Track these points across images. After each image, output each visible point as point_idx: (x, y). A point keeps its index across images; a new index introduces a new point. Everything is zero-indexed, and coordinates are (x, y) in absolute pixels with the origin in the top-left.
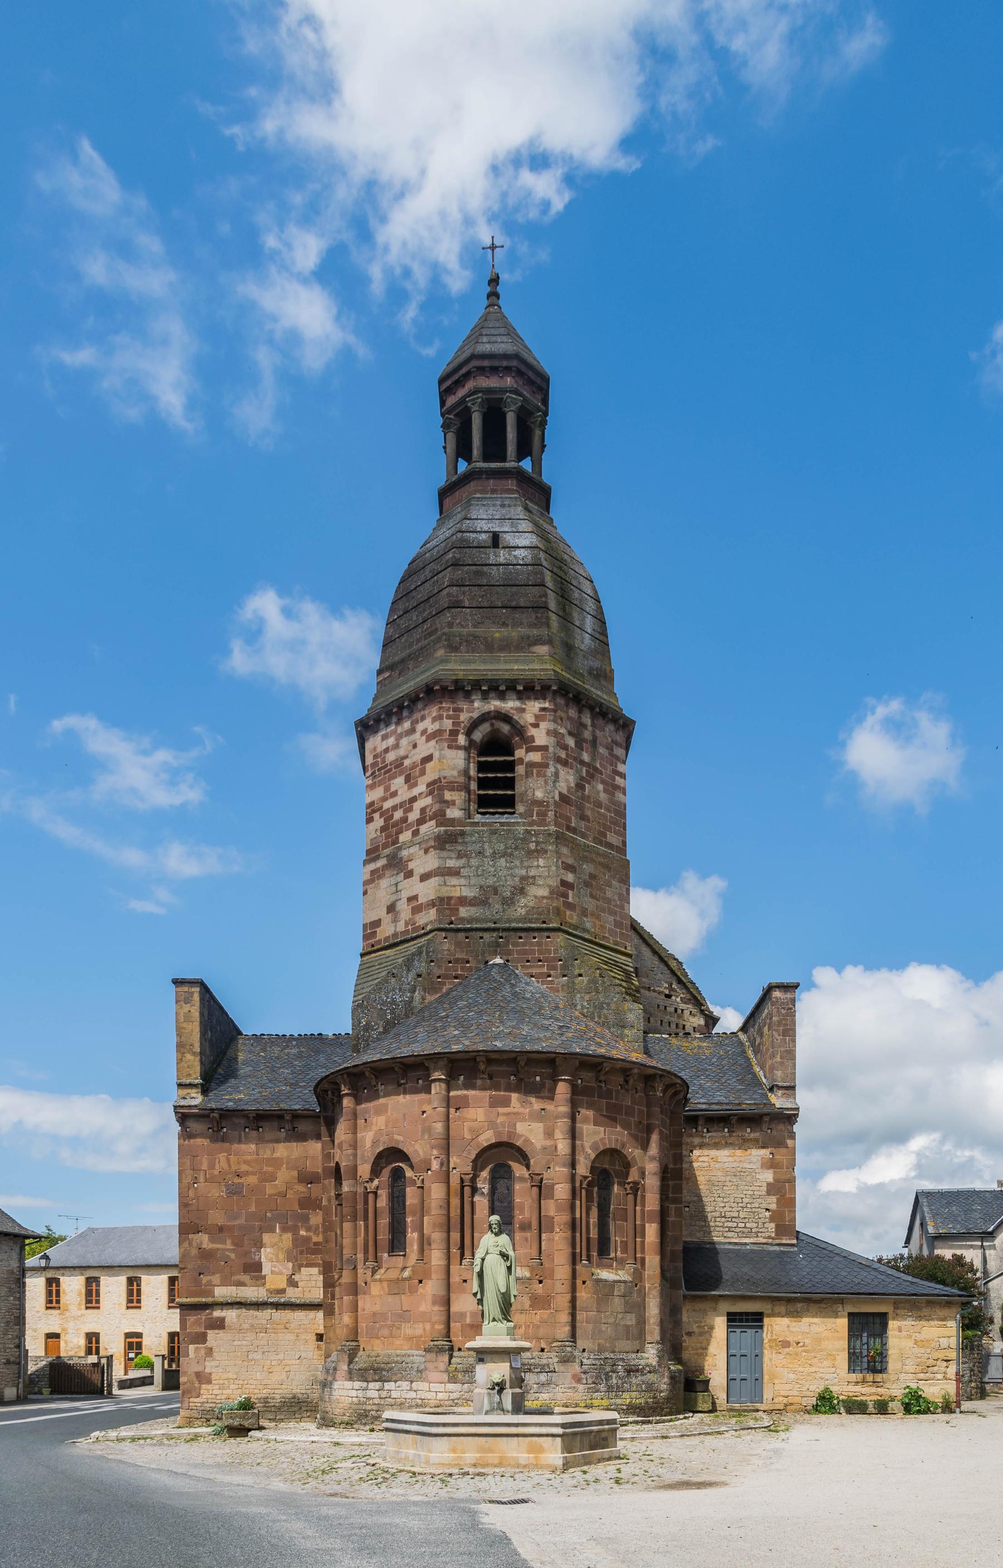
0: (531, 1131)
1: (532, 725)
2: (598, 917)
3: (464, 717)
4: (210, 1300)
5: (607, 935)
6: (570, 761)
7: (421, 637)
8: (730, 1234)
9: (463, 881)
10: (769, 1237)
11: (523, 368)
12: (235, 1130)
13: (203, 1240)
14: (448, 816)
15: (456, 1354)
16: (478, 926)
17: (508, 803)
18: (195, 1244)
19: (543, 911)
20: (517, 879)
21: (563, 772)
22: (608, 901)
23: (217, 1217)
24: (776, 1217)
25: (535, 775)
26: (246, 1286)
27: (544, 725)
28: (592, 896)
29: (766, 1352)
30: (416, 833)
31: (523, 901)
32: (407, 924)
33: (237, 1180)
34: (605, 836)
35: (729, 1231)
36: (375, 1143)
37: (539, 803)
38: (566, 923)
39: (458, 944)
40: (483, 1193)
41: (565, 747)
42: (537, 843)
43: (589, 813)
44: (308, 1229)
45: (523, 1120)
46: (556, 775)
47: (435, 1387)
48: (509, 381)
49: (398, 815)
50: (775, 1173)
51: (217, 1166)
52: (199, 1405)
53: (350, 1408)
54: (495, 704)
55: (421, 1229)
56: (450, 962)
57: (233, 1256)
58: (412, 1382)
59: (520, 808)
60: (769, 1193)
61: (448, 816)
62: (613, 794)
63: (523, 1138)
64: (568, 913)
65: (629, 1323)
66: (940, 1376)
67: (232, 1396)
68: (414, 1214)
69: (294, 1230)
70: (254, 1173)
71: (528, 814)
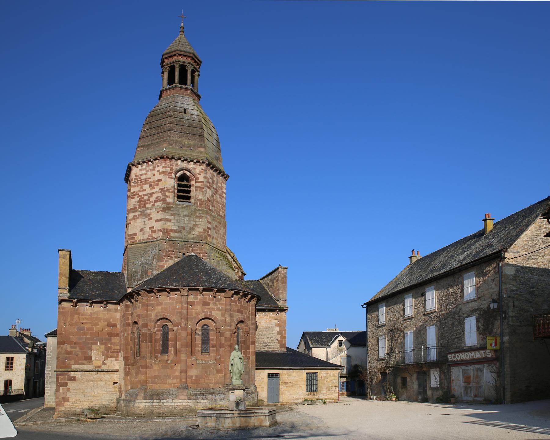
0: (217, 314)
1: (198, 174)
2: (217, 240)
3: (174, 168)
4: (70, 370)
5: (219, 246)
6: (210, 187)
7: (157, 139)
8: (265, 348)
9: (172, 224)
10: (278, 349)
11: (194, 57)
12: (82, 307)
13: (67, 347)
14: (167, 201)
15: (190, 389)
16: (178, 240)
17: (188, 198)
18: (64, 349)
19: (201, 236)
20: (192, 225)
21: (208, 190)
22: (220, 234)
23: (73, 338)
24: (280, 342)
25: (199, 190)
26: (85, 365)
27: (203, 175)
28: (216, 233)
29: (280, 386)
30: (153, 205)
31: (194, 233)
32: (149, 236)
33: (82, 325)
34: (219, 213)
35: (265, 347)
36: (156, 316)
37: (200, 200)
38: (208, 241)
39: (170, 245)
40: (199, 335)
41: (209, 182)
42: (199, 213)
43: (215, 205)
44: (111, 344)
45: (215, 310)
46: (206, 191)
47: (182, 401)
48: (189, 60)
49: (146, 198)
50: (279, 328)
51: (74, 319)
52: (63, 410)
53: (144, 409)
54: (185, 165)
55: (175, 346)
56: (167, 251)
57: (80, 353)
58: (173, 400)
59: (193, 201)
60: (278, 334)
61: (167, 201)
62: (222, 199)
63: (214, 317)
64: (209, 238)
65: (246, 378)
66: (333, 392)
67: (77, 406)
68: (172, 341)
69: (106, 344)
70: (90, 323)
71: (196, 203)
